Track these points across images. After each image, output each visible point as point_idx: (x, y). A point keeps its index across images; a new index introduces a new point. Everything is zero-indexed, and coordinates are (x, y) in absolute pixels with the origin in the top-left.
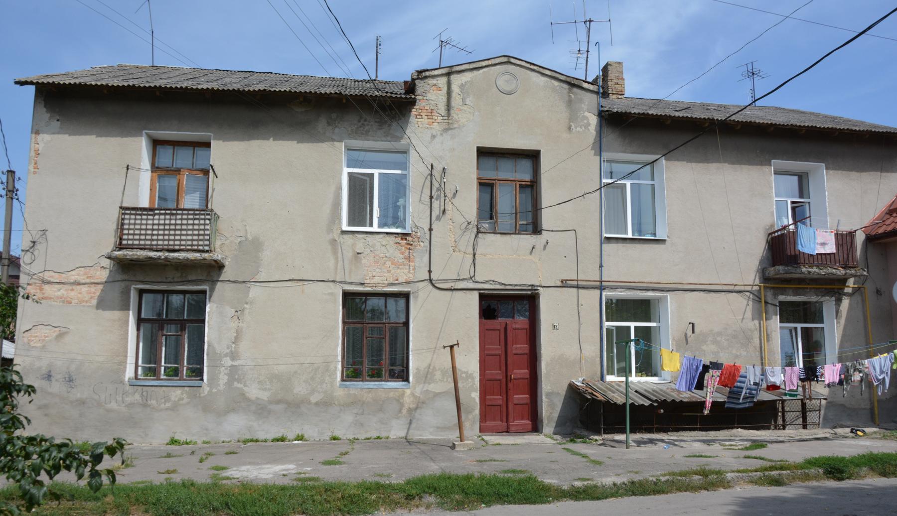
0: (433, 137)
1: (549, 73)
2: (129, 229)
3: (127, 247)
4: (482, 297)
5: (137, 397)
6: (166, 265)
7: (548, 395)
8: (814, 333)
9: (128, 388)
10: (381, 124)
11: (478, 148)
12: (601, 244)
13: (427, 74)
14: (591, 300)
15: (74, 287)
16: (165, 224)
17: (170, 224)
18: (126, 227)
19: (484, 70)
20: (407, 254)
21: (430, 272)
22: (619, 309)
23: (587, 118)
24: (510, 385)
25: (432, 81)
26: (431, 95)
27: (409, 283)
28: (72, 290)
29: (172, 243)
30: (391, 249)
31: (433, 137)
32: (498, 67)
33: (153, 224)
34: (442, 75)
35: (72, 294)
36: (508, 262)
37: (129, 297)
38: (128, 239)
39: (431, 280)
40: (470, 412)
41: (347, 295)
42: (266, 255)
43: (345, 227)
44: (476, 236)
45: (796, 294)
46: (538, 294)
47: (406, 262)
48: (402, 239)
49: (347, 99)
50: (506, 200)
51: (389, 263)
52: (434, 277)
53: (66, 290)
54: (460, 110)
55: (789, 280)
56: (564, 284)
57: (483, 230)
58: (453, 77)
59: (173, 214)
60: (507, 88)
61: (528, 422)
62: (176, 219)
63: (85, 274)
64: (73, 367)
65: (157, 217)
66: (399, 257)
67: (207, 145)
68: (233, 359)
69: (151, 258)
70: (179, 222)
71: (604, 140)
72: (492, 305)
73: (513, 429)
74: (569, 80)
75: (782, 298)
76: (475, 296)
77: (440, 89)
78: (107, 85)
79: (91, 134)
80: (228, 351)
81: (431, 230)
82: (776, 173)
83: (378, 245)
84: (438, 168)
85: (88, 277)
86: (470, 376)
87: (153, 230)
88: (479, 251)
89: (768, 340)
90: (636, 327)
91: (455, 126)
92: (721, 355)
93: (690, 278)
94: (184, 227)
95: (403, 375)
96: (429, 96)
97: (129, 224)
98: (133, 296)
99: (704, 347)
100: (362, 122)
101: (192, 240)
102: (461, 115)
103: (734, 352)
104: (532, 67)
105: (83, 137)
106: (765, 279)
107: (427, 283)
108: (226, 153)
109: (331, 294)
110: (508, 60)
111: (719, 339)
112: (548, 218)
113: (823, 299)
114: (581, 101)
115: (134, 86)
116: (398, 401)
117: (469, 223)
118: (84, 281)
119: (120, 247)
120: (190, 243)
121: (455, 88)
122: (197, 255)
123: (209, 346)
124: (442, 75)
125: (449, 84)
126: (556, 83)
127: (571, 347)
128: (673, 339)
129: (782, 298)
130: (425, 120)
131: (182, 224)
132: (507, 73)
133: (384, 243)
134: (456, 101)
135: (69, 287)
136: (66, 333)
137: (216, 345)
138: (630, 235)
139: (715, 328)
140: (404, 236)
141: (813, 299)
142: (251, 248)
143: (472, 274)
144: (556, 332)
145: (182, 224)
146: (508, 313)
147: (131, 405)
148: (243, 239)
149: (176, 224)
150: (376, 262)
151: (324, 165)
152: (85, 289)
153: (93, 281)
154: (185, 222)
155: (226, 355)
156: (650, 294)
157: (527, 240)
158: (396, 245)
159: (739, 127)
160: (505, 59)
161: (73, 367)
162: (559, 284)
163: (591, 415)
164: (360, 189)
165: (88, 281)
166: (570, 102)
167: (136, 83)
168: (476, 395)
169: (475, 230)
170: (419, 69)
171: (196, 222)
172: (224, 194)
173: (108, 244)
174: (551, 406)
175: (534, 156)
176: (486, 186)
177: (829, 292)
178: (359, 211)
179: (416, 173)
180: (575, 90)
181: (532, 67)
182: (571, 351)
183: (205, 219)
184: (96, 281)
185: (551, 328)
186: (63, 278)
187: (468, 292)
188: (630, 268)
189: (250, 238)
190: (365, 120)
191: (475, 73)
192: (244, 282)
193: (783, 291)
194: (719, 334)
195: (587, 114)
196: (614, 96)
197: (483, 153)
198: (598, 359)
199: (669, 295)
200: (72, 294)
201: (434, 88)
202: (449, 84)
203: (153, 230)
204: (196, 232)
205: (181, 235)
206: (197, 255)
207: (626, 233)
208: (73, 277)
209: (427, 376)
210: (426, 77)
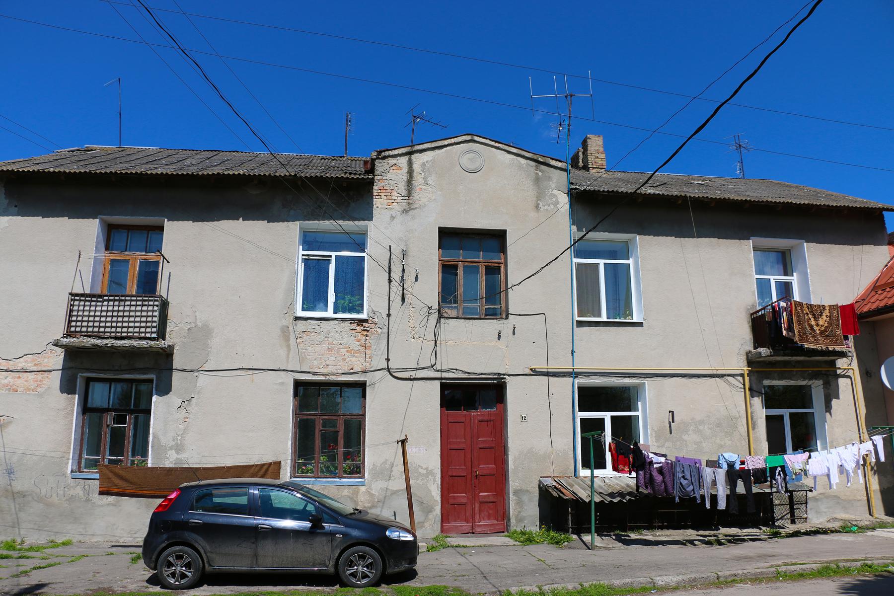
0: (393, 218)
2: (77, 321)
3: (80, 334)
4: (444, 387)
5: (79, 491)
6: (114, 353)
7: (516, 492)
9: (70, 481)
11: (505, 232)
13: (387, 153)
14: (564, 391)
15: (21, 374)
16: (113, 311)
17: (118, 311)
18: (75, 313)
19: (449, 148)
20: (363, 341)
21: (388, 360)
22: (590, 398)
25: (392, 161)
27: (365, 372)
28: (19, 377)
29: (119, 330)
30: (346, 335)
31: (393, 218)
33: (102, 311)
35: (19, 382)
36: (472, 348)
37: (76, 386)
38: (76, 326)
39: (389, 370)
40: (428, 510)
41: (298, 384)
42: (215, 342)
43: (300, 313)
44: (438, 322)
45: (780, 379)
46: (505, 383)
47: (363, 349)
48: (358, 325)
49: (303, 181)
51: (343, 351)
52: (392, 365)
53: (13, 378)
55: (787, 366)
57: (445, 315)
58: (414, 157)
59: (122, 300)
60: (472, 167)
62: (124, 306)
63: (33, 361)
64: (15, 459)
65: (105, 303)
66: (354, 345)
67: (161, 228)
68: (177, 453)
69: (97, 345)
70: (127, 308)
75: (766, 382)
76: (437, 384)
78: (65, 172)
79: (263, 220)
80: (174, 443)
81: (389, 315)
82: (755, 249)
83: (333, 332)
84: (397, 251)
85: (35, 365)
86: (430, 473)
87: (101, 316)
89: (754, 428)
90: (612, 417)
92: (704, 445)
93: (669, 366)
94: (132, 314)
95: (357, 471)
97: (77, 316)
98: (80, 383)
99: (685, 437)
101: (140, 327)
102: (421, 195)
103: (718, 441)
105: (175, 222)
106: (751, 362)
108: (180, 237)
109: (282, 384)
111: (701, 427)
112: (516, 300)
113: (810, 383)
115: (90, 172)
116: (351, 499)
117: (430, 308)
118: (31, 369)
119: (68, 335)
120: (137, 330)
121: (416, 167)
122: (144, 343)
123: (154, 437)
125: (410, 164)
127: (541, 439)
128: (652, 429)
129: (766, 382)
130: (384, 200)
131: (130, 311)
132: (469, 151)
133: (339, 330)
134: (418, 180)
135: (17, 375)
136: (10, 422)
137: (161, 437)
138: (604, 318)
139: (705, 422)
140: (361, 322)
141: (804, 383)
142: (201, 334)
144: (524, 424)
145: (130, 311)
146: (472, 401)
147: (71, 499)
148: (193, 325)
149: (124, 311)
150: (330, 350)
151: (274, 249)
152: (31, 376)
153: (40, 368)
154: (133, 308)
155: (171, 448)
156: (627, 381)
157: (491, 326)
159: (680, 202)
160: (468, 138)
161: (15, 459)
162: (528, 372)
163: (563, 514)
164: (315, 272)
165: (35, 369)
166: (537, 180)
167: (92, 169)
168: (435, 492)
171: (145, 308)
172: (173, 282)
173: (58, 331)
174: (525, 511)
176: (448, 269)
177: (815, 376)
178: (314, 295)
179: (373, 256)
180: (543, 167)
182: (541, 445)
183: (154, 305)
184: (44, 369)
185: (520, 419)
186: (11, 365)
188: (606, 354)
189: (200, 324)
191: (437, 152)
192: (191, 371)
193: (768, 376)
194: (701, 422)
195: (555, 192)
196: (595, 170)
199: (647, 382)
200: (19, 382)
201: (394, 168)
202: (410, 164)
203: (101, 316)
204: (144, 319)
205: (129, 322)
206: (144, 343)
207: (599, 316)
208: (21, 364)
209: (385, 473)
210: (385, 158)
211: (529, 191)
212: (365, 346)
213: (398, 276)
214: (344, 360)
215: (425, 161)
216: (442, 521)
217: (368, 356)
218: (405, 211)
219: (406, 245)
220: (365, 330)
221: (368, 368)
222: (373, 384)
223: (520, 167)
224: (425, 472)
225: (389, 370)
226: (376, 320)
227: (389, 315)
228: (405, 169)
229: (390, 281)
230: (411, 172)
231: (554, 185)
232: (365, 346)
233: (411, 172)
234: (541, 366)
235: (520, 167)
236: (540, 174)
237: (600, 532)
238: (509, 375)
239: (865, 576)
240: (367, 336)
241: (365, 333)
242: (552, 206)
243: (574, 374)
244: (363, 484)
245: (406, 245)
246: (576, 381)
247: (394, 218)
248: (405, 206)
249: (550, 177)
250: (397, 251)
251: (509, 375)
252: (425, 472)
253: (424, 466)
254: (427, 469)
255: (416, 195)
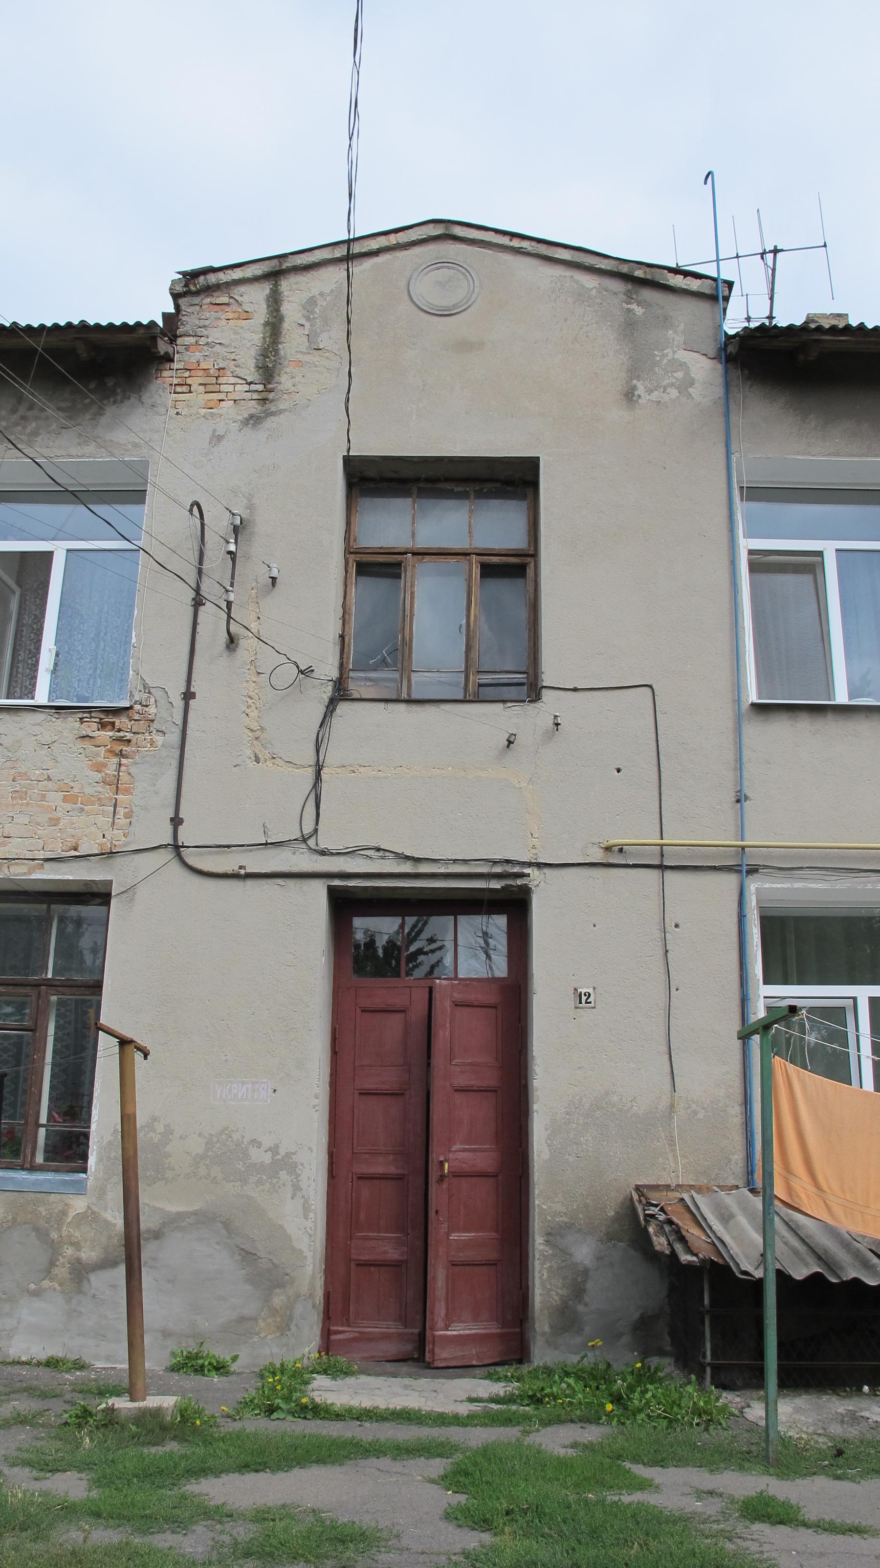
0: (217, 438)
1: (565, 255)
8: (523, 497)
10: (72, 413)
11: (533, 464)
12: (738, 731)
13: (212, 278)
14: (711, 920)
20: (111, 770)
21: (176, 821)
23: (683, 365)
24: (438, 1195)
26: (229, 335)
27: (110, 854)
32: (417, 250)
34: (256, 279)
36: (426, 791)
39: (177, 847)
44: (333, 703)
47: (107, 792)
48: (103, 726)
50: (437, 613)
51: (55, 798)
54: (300, 364)
56: (614, 859)
58: (286, 285)
61: (391, 1327)
66: (88, 781)
71: (733, 418)
72: (382, 927)
73: (443, 1354)
74: (625, 269)
76: (317, 896)
77: (247, 316)
81: (188, 696)
84: (218, 523)
86: (285, 1163)
88: (332, 756)
91: (282, 407)
96: (214, 335)
100: (22, 410)
104: (516, 243)
107: (167, 855)
110: (446, 232)
114: (666, 322)
117: (306, 672)
121: (291, 310)
124: (256, 279)
125: (275, 301)
126: (590, 282)
130: (199, 397)
133: (47, 738)
134: (293, 343)
143: (308, 828)
144: (586, 1015)
157: (493, 720)
158: (80, 744)
160: (438, 230)
162: (597, 856)
166: (629, 328)
169: (328, 691)
170: (188, 268)
175: (515, 480)
176: (375, 567)
180: (647, 294)
181: (516, 243)
182: (639, 1085)
185: (571, 1001)
187: (291, 883)
190: (31, 407)
195: (683, 356)
197: (370, 479)
198: (735, 1110)
202: (275, 301)
211: (607, 357)
212: (116, 784)
213: (220, 568)
214: (54, 822)
215: (315, 292)
216: (328, 1316)
217: (121, 811)
218: (254, 421)
219: (251, 507)
220: (120, 740)
221: (120, 841)
222: (130, 890)
223: (581, 295)
224: (267, 1158)
225: (177, 847)
226: (152, 710)
227: (188, 696)
228: (261, 314)
229: (198, 602)
230: (274, 327)
231: (679, 339)
232: (116, 784)
233: (274, 327)
234: (640, 834)
235: (581, 295)
236: (639, 311)
237: (794, 1380)
238: (539, 865)
239: (471, 1329)
240: (121, 754)
241: (117, 748)
242: (674, 393)
243: (742, 867)
244: (80, 1189)
245: (251, 507)
246: (753, 885)
247: (220, 438)
248: (253, 407)
249: (666, 318)
250: (218, 523)
251: (539, 865)
252: (267, 1158)
253: (267, 1142)
254: (274, 1150)
255: (284, 381)
